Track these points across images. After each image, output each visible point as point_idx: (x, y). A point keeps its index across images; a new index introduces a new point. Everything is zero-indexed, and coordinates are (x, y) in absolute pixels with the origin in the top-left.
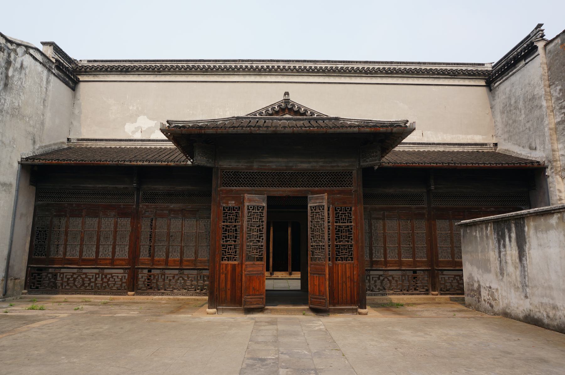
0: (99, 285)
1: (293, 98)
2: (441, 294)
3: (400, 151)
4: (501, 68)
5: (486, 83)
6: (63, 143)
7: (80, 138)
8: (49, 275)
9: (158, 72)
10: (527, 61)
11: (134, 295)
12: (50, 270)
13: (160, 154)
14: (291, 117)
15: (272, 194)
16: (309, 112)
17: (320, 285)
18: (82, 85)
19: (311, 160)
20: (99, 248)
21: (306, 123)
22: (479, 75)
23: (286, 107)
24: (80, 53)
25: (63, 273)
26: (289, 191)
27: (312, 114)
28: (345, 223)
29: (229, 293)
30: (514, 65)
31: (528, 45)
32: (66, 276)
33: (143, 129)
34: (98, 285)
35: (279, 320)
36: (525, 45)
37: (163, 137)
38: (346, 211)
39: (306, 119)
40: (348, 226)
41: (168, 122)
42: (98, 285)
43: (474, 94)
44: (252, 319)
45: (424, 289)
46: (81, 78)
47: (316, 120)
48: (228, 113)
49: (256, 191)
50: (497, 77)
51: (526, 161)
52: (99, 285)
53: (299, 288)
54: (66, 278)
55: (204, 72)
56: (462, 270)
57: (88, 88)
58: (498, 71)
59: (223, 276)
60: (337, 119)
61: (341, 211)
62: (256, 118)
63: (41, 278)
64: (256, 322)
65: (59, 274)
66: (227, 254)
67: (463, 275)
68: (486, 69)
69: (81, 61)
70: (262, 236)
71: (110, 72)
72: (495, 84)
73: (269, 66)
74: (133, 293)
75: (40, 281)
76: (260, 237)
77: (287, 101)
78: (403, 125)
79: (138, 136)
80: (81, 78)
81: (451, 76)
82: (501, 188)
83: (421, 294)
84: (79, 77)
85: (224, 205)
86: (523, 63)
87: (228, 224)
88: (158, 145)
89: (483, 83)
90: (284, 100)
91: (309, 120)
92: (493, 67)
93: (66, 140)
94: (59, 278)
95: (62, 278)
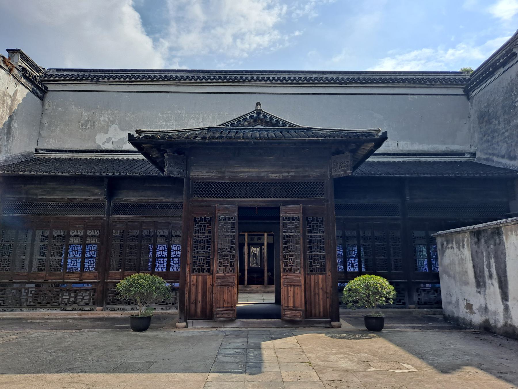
0: (66, 300)
1: (264, 108)
2: (419, 308)
3: (374, 162)
4: (479, 77)
5: (463, 91)
6: (32, 153)
7: (49, 147)
8: (14, 291)
9: (129, 82)
10: (506, 68)
11: (102, 310)
12: (15, 286)
13: (132, 165)
14: (262, 127)
15: (243, 204)
16: (281, 122)
17: (293, 296)
18: (49, 94)
19: (283, 170)
20: (67, 262)
21: (278, 133)
22: (457, 83)
23: (259, 117)
24: (47, 61)
25: (28, 289)
26: (260, 202)
27: (284, 124)
28: (317, 233)
29: (199, 305)
30: (492, 73)
31: (506, 52)
32: (31, 291)
33: (115, 140)
34: (64, 300)
35: (250, 333)
36: (504, 52)
37: (130, 147)
38: (318, 221)
39: (278, 129)
40: (320, 237)
41: (137, 131)
42: (64, 300)
43: (443, 104)
44: (223, 331)
45: (400, 302)
46: (50, 87)
47: (288, 130)
48: (202, 124)
49: (227, 201)
50: (475, 86)
51: (505, 169)
52: (66, 300)
53: (274, 301)
54: (31, 293)
55: (177, 83)
56: (439, 283)
57: (59, 97)
58: (475, 80)
59: (193, 289)
60: (309, 129)
61: (312, 221)
62: (227, 129)
63: (4, 294)
64: (226, 335)
65: (23, 289)
66: (206, 225)
67: (440, 288)
68: (464, 77)
69: (49, 69)
70: (233, 247)
71: (80, 81)
72: (473, 92)
73: (242, 77)
74: (101, 308)
75: (4, 297)
76: (232, 247)
77: (259, 112)
78: (374, 133)
79: (109, 146)
80: (50, 87)
81: (428, 85)
82: (468, 196)
83: (398, 308)
84: (47, 86)
85: (195, 216)
86: (502, 70)
87: (199, 234)
88: (131, 157)
89: (461, 91)
90: (256, 110)
91: (281, 131)
92: (471, 76)
93: (34, 151)
94: (23, 294)
95: (27, 294)
